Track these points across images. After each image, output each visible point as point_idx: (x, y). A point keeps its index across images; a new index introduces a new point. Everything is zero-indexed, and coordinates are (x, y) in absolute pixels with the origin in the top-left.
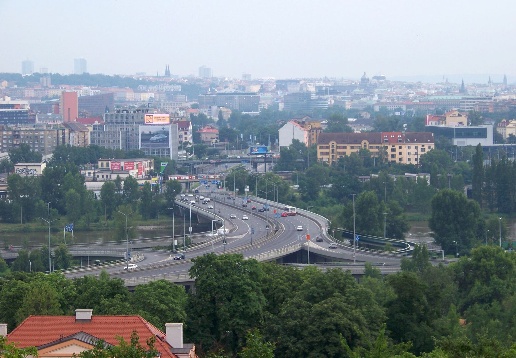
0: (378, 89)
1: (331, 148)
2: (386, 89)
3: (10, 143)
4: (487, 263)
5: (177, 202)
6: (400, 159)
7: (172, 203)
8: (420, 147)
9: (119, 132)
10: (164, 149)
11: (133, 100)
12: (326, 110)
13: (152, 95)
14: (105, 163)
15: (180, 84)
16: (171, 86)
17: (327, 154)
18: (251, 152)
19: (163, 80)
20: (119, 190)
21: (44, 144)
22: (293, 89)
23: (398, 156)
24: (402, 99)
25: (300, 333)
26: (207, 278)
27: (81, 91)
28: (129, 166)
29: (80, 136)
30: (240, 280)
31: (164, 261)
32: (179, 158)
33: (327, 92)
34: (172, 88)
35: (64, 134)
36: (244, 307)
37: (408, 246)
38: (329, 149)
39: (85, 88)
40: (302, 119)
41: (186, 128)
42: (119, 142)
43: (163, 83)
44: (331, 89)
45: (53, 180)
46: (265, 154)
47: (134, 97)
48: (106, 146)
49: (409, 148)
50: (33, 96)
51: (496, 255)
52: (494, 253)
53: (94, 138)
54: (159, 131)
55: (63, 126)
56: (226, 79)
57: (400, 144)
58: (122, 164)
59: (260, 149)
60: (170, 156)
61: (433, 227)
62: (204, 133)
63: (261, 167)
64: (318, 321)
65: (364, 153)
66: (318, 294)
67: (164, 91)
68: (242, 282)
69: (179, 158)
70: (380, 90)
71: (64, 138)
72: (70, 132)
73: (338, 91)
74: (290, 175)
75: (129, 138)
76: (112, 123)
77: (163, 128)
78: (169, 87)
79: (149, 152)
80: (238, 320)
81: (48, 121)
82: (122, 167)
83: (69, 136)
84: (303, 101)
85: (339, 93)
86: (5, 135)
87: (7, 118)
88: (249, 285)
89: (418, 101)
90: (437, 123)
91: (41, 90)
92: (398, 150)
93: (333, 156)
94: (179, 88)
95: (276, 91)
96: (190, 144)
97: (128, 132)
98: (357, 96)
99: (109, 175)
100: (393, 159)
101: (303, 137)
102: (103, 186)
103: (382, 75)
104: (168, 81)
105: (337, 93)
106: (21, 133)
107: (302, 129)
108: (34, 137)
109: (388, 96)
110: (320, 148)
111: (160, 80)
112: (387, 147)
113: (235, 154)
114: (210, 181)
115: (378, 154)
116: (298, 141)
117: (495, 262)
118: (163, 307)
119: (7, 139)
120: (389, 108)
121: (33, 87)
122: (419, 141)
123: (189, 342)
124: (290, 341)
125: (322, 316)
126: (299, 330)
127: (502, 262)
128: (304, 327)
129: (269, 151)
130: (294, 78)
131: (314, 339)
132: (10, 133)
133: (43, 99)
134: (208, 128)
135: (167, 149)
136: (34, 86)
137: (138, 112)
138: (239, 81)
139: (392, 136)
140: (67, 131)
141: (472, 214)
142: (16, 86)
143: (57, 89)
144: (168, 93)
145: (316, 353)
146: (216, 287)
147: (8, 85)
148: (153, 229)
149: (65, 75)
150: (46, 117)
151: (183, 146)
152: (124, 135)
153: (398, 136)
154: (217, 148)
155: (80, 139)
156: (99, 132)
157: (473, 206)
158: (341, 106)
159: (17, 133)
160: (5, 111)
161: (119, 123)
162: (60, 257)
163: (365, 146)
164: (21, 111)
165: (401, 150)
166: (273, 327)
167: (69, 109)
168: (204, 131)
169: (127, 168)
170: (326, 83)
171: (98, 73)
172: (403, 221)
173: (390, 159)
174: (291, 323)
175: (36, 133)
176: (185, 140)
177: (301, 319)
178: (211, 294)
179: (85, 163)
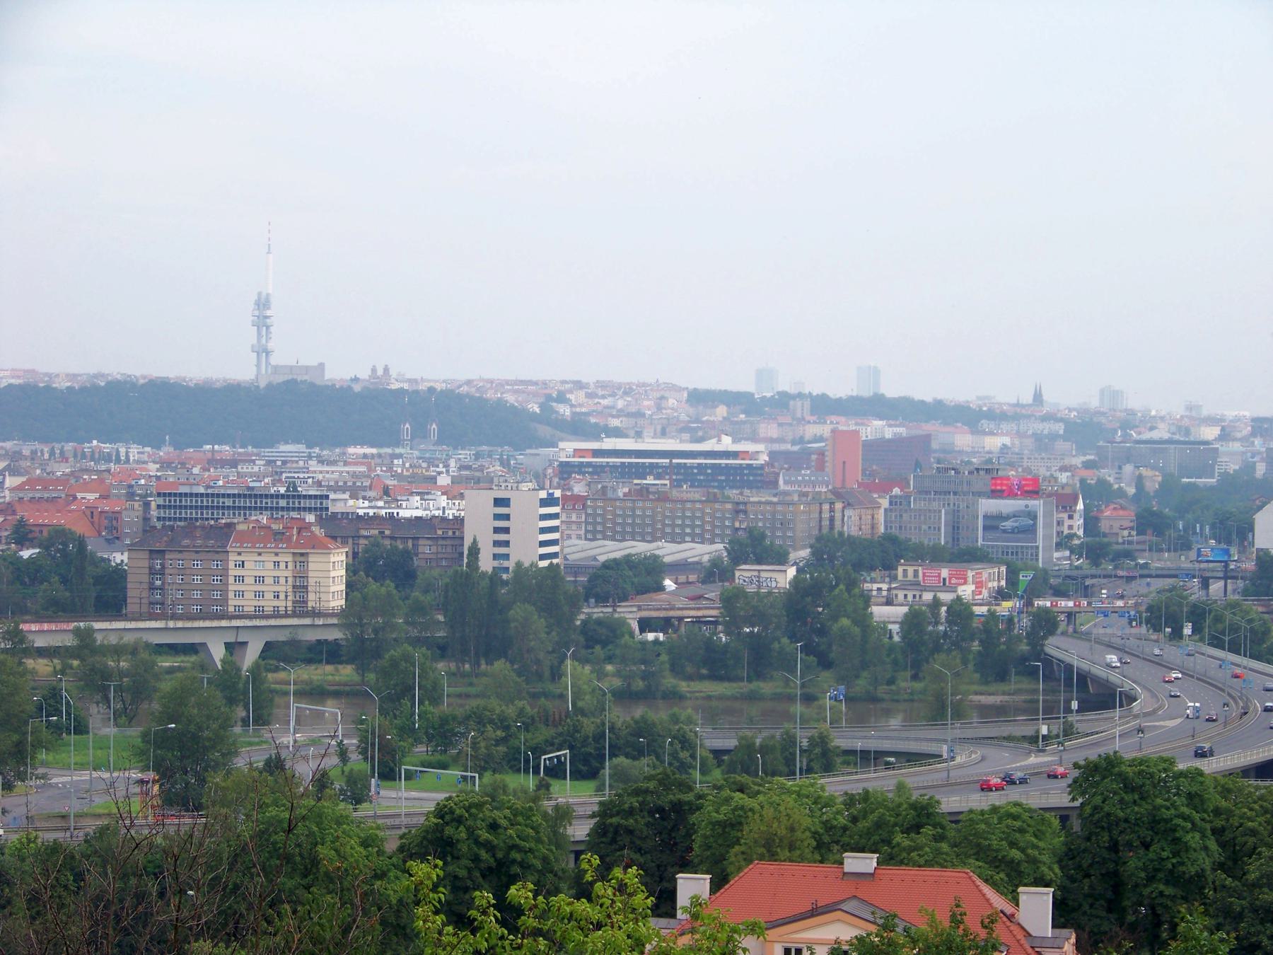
5: (1049, 650)
7: (1038, 653)
9: (940, 511)
11: (969, 449)
13: (1007, 440)
14: (910, 570)
15: (1061, 420)
20: (937, 623)
26: (1103, 802)
27: (869, 428)
28: (956, 578)
29: (863, 517)
30: (1168, 809)
32: (1055, 565)
34: (1047, 428)
35: (834, 512)
36: (1174, 861)
41: (1071, 507)
42: (939, 529)
43: (1029, 417)
45: (809, 599)
50: (775, 436)
55: (833, 497)
56: (1153, 413)
58: (945, 573)
60: (1037, 560)
62: (1108, 518)
63: (1216, 587)
67: (1030, 432)
68: (1173, 811)
69: (1055, 565)
71: (832, 519)
72: (844, 508)
75: (958, 522)
76: (927, 493)
77: (1027, 506)
80: (1162, 887)
82: (944, 579)
83: (843, 516)
87: (723, 478)
91: (790, 425)
94: (1060, 428)
95: (1252, 439)
96: (1079, 538)
97: (958, 511)
106: (749, 507)
111: (1023, 411)
114: (1116, 612)
118: (1015, 854)
119: (723, 519)
121: (775, 419)
123: (1064, 926)
132: (729, 506)
133: (793, 443)
134: (1115, 509)
135: (1032, 547)
137: (978, 472)
138: (1178, 417)
140: (839, 506)
142: (742, 416)
143: (823, 423)
144: (1038, 438)
147: (728, 413)
148: (1001, 701)
149: (838, 396)
150: (800, 478)
151: (1064, 542)
159: (741, 507)
160: (720, 464)
161: (940, 493)
162: (818, 750)
164: (752, 464)
167: (844, 463)
168: (1107, 513)
169: (954, 581)
175: (779, 508)
178: (1110, 831)
179: (873, 568)
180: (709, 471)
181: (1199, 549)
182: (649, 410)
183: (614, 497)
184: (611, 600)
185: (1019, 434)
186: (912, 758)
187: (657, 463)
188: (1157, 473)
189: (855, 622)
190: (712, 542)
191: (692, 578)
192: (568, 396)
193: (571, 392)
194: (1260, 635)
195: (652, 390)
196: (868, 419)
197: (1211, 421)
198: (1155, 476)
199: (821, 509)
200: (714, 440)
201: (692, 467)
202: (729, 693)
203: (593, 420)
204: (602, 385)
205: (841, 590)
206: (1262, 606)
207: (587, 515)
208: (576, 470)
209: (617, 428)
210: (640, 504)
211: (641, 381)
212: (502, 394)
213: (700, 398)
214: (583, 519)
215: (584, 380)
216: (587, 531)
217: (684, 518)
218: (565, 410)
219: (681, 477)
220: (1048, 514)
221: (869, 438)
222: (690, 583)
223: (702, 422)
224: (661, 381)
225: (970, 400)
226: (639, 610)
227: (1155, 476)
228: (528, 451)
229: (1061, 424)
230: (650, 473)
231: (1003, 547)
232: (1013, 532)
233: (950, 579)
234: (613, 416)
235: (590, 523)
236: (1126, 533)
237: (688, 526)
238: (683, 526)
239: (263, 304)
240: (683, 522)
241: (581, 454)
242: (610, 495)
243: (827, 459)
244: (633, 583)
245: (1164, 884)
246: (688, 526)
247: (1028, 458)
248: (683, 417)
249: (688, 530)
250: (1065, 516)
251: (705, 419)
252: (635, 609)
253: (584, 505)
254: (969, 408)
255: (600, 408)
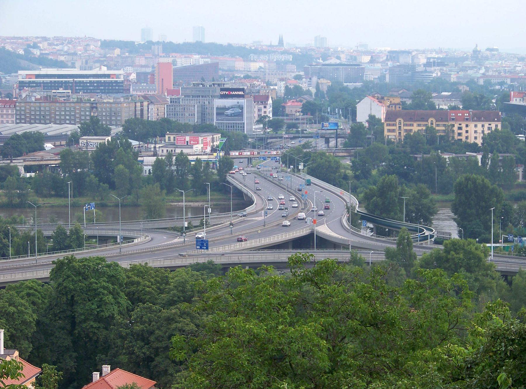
0: (488, 62)
1: (398, 126)
2: (497, 62)
3: (88, 115)
4: (455, 255)
6: (467, 138)
8: (486, 125)
9: (194, 106)
10: (239, 123)
11: (243, 69)
12: (429, 83)
13: (262, 64)
14: (172, 137)
15: (291, 53)
16: (283, 55)
17: (393, 131)
18: (323, 127)
19: (275, 50)
20: (171, 165)
21: (120, 116)
22: (404, 60)
23: (464, 134)
24: (508, 72)
25: (148, 338)
26: (63, 281)
27: (191, 59)
28: (193, 141)
29: (159, 109)
30: (96, 283)
31: (170, 243)
32: (254, 132)
33: (434, 64)
34: (283, 58)
36: (98, 310)
37: (424, 230)
38: (396, 126)
39: (195, 56)
40: (398, 91)
41: (265, 102)
43: (275, 52)
44: (439, 61)
46: (336, 130)
47: (243, 66)
48: (182, 121)
49: (476, 126)
50: (143, 64)
51: (466, 248)
52: (464, 246)
53: (170, 112)
54: (233, 105)
55: (142, 99)
56: (339, 49)
57: (467, 123)
58: (187, 139)
59: (331, 124)
60: (244, 130)
61: (455, 210)
62: (289, 107)
63: (332, 143)
64: (165, 327)
65: (430, 130)
66: (179, 298)
67: (275, 60)
68: (99, 285)
69: (254, 132)
70: (490, 62)
71: (142, 110)
72: (148, 104)
73: (446, 63)
74: (352, 152)
75: (204, 111)
76: (188, 96)
77: (238, 103)
78: (281, 57)
79: (224, 126)
80: (92, 323)
81: (142, 91)
82: (187, 142)
83: (148, 108)
84: (407, 73)
85: (446, 65)
86: (68, 107)
87: (102, 88)
88: (104, 288)
89: (523, 75)
90: (522, 99)
91: (151, 58)
92: (464, 129)
93: (400, 133)
94: (290, 58)
95: (387, 62)
96: (269, 117)
97: (204, 106)
98: (464, 69)
99: (173, 149)
100: (460, 138)
101: (381, 113)
102: (155, 162)
103: (495, 47)
104: (279, 51)
105: (444, 65)
106: (98, 105)
107: (380, 104)
108: (111, 109)
109: (495, 69)
110: (387, 125)
111: (273, 50)
112: (454, 126)
113: (310, 129)
114: (270, 157)
115: (445, 132)
116: (374, 116)
117: (464, 255)
118: (12, 309)
119: (85, 111)
120: (493, 81)
121: (144, 55)
122: (486, 120)
124: (136, 346)
125: (170, 322)
126: (146, 335)
127: (471, 256)
128: (152, 333)
129: (341, 127)
130: (407, 50)
131: (159, 345)
132: (88, 105)
134: (293, 102)
135: (241, 124)
136: (145, 54)
137: (214, 85)
138: (352, 51)
139: (459, 115)
140: (145, 104)
141: (495, 199)
142: (127, 54)
143: (168, 57)
144: (278, 63)
145: (161, 358)
146: (71, 290)
147: (121, 52)
148: (201, 205)
149: (178, 43)
150: (141, 88)
151: (261, 120)
152: (200, 109)
153: (466, 115)
154: (297, 121)
155: (159, 111)
156: (175, 106)
157: (496, 191)
158: (445, 79)
159: (94, 105)
160: (101, 81)
161: (195, 96)
162: (74, 237)
163: (432, 124)
164: (117, 81)
165: (468, 129)
166: (121, 331)
167: (162, 79)
168: (289, 104)
169: (192, 142)
170: (438, 54)
171: (211, 42)
172: (430, 205)
173: (456, 137)
174: (138, 328)
175: (113, 105)
176: (264, 113)
177: (149, 325)
178: (67, 296)
180: (95, 85)
181: (323, 124)
182: (80, 51)
183: (29, 101)
184: (9, 157)
185: (269, 61)
186: (104, 240)
187: (68, 81)
188: (329, 81)
189: (127, 166)
190: (75, 124)
191: (64, 143)
192: (38, 45)
193: (40, 42)
194: (334, 169)
195: (82, 41)
196: (191, 55)
197: (366, 53)
198: (328, 83)
199: (136, 105)
200: (98, 69)
201: (87, 83)
202: (63, 204)
203: (50, 57)
204: (57, 39)
205: (121, 150)
206: (347, 152)
207: (16, 110)
208: (27, 85)
209: (62, 62)
210: (43, 104)
211: (77, 36)
212: (4, 44)
213: (107, 45)
214: (15, 113)
215: (48, 36)
216: (17, 119)
217: (65, 111)
218: (37, 52)
219: (81, 88)
220: (249, 106)
221: (192, 64)
222: (62, 145)
223: (107, 58)
224: (87, 36)
225: (246, 43)
226: (24, 161)
227: (328, 83)
228: (12, 74)
229: (291, 56)
230: (61, 87)
231: (226, 123)
232: (231, 116)
233: (190, 141)
234: (61, 55)
235: (18, 115)
236: (298, 114)
237: (68, 115)
238: (65, 115)
239: (329, 202)
240: (65, 113)
241: (30, 77)
242: (28, 100)
243: (155, 77)
244: (26, 147)
245: (93, 322)
246: (68, 115)
247: (268, 74)
248: (97, 55)
249: (68, 117)
250: (262, 106)
251: (108, 56)
252: (22, 161)
253: (15, 106)
254: (245, 48)
255: (55, 51)
